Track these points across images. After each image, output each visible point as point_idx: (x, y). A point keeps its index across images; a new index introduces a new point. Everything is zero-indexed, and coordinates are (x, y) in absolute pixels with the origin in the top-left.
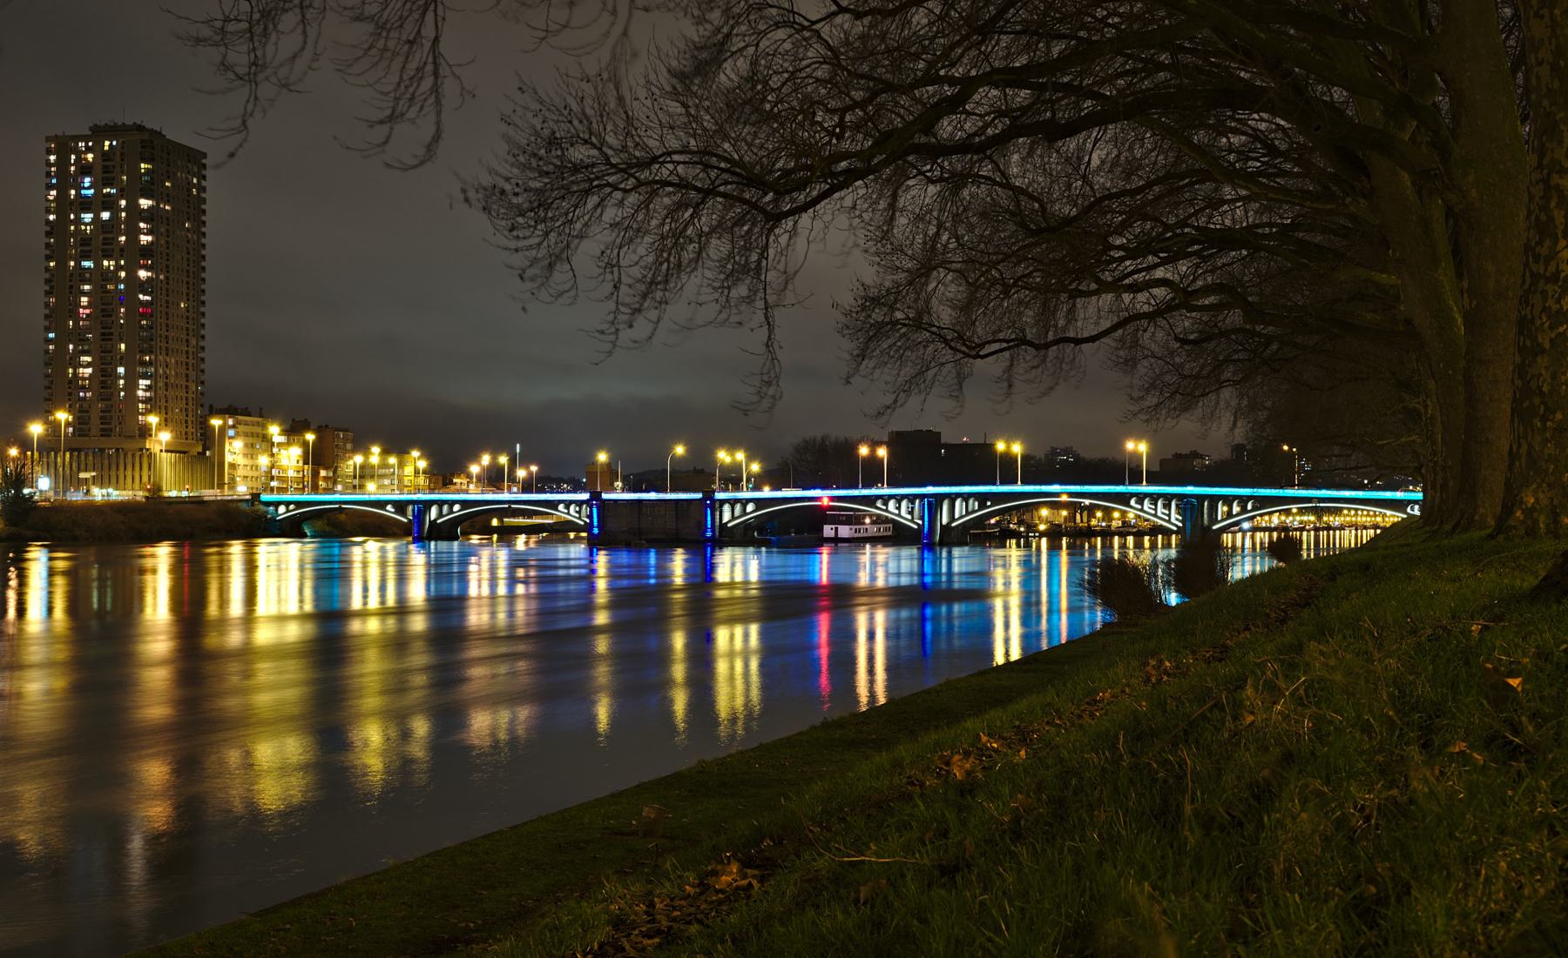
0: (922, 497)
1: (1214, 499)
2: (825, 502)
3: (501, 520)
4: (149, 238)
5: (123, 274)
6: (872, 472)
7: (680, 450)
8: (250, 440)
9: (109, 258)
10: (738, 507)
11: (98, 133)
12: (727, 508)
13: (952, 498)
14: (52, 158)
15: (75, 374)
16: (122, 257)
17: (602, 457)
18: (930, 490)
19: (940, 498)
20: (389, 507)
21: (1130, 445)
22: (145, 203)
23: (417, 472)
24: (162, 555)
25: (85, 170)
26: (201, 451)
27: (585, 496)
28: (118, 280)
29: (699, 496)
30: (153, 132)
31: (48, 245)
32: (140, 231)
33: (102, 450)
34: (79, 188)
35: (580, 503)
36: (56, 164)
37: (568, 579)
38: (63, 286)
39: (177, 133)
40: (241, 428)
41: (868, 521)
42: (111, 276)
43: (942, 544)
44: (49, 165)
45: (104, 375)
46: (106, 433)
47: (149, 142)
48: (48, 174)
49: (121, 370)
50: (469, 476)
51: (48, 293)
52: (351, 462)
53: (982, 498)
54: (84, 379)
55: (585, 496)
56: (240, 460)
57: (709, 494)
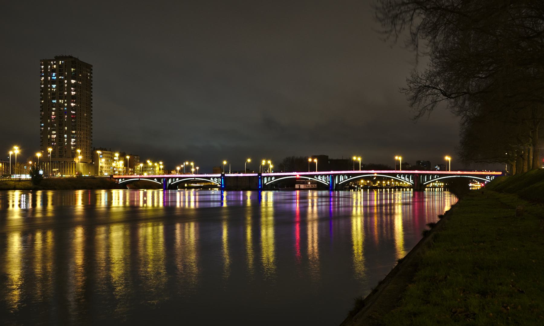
0: (329, 175)
1: (424, 175)
2: (298, 176)
4: (75, 93)
5: (66, 105)
7: (249, 160)
8: (107, 159)
10: (269, 178)
12: (265, 179)
14: (42, 67)
15: (50, 137)
16: (66, 99)
17: (225, 163)
18: (332, 172)
19: (335, 175)
20: (155, 179)
21: (397, 158)
22: (73, 81)
23: (160, 169)
24: (80, 193)
25: (53, 71)
26: (91, 161)
27: (219, 175)
28: (65, 107)
29: (257, 175)
30: (75, 58)
31: (41, 95)
32: (72, 91)
33: (59, 162)
34: (51, 76)
35: (218, 178)
37: (214, 201)
38: (46, 108)
39: (83, 58)
40: (104, 155)
41: (309, 183)
43: (336, 190)
44: (41, 69)
45: (60, 137)
46: (61, 156)
47: (73, 61)
48: (41, 72)
49: (66, 136)
50: (176, 171)
52: (139, 166)
53: (349, 175)
54: (53, 139)
55: (219, 175)
56: (104, 165)
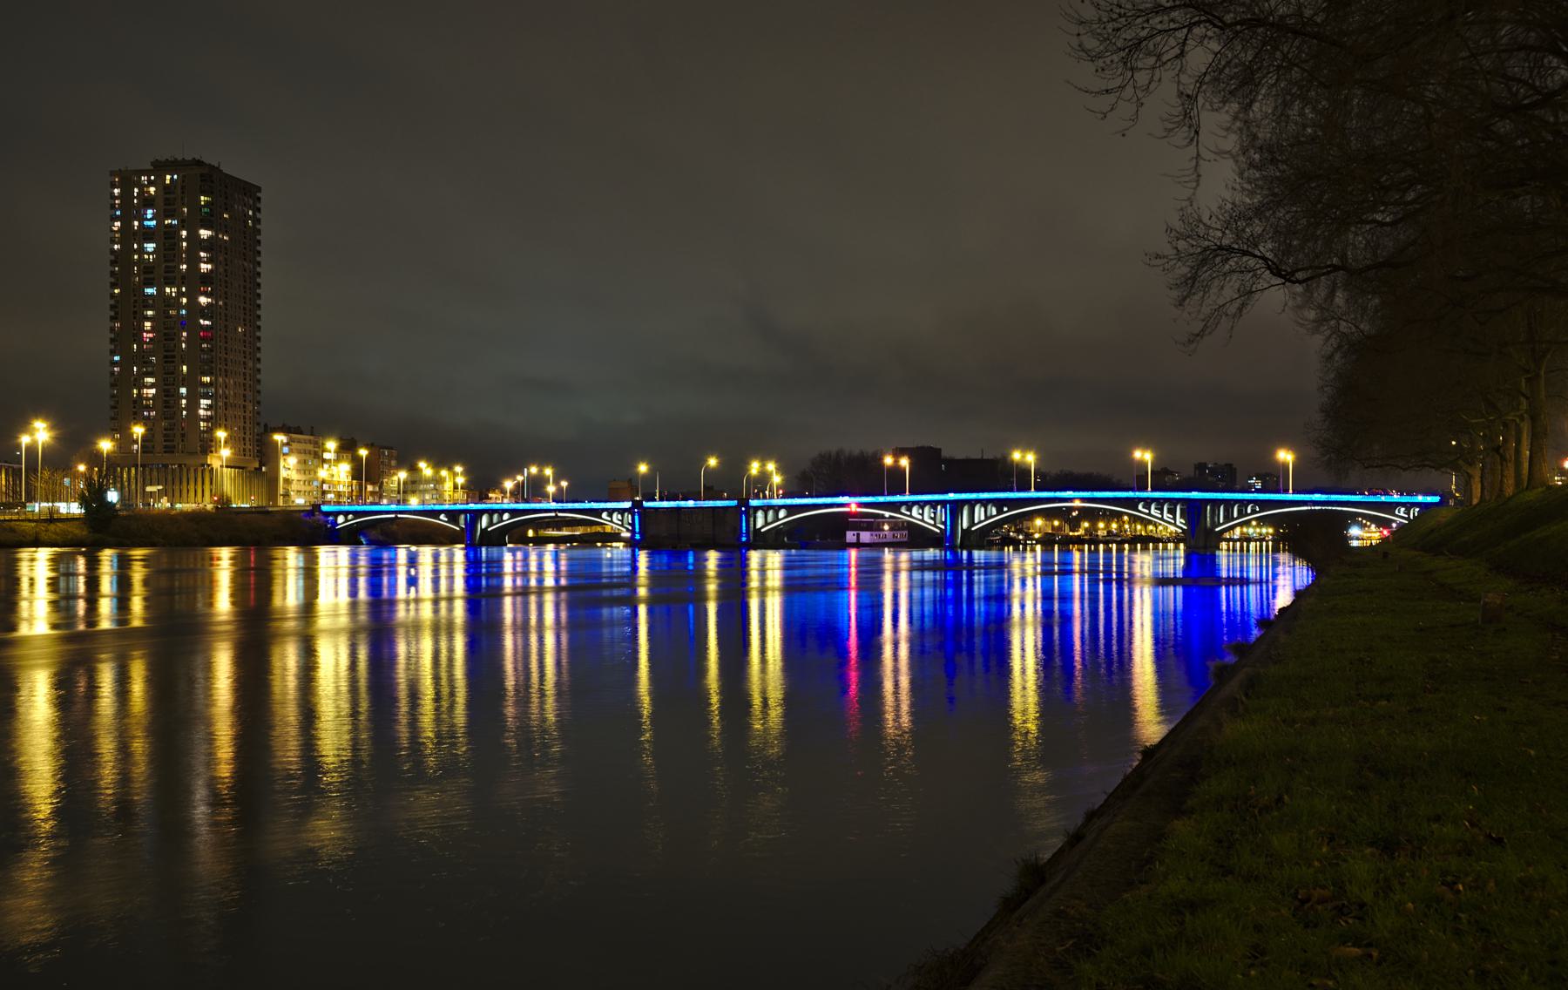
2: (854, 508)
3: (536, 531)
5: (185, 300)
6: (895, 482)
7: (713, 462)
8: (303, 457)
9: (171, 285)
11: (160, 168)
13: (972, 504)
15: (139, 394)
16: (183, 284)
17: (643, 468)
18: (951, 496)
20: (442, 517)
22: (205, 233)
23: (455, 487)
25: (148, 202)
26: (258, 462)
27: (628, 505)
28: (180, 306)
31: (113, 273)
32: (200, 260)
34: (142, 219)
35: (622, 511)
36: (120, 197)
38: (127, 310)
40: (294, 445)
41: (886, 527)
42: (173, 303)
44: (114, 197)
46: (170, 450)
47: (205, 176)
48: (113, 207)
50: (503, 492)
51: (113, 319)
53: (999, 504)
54: (148, 399)
55: (628, 505)
56: (294, 475)
57: (744, 502)
